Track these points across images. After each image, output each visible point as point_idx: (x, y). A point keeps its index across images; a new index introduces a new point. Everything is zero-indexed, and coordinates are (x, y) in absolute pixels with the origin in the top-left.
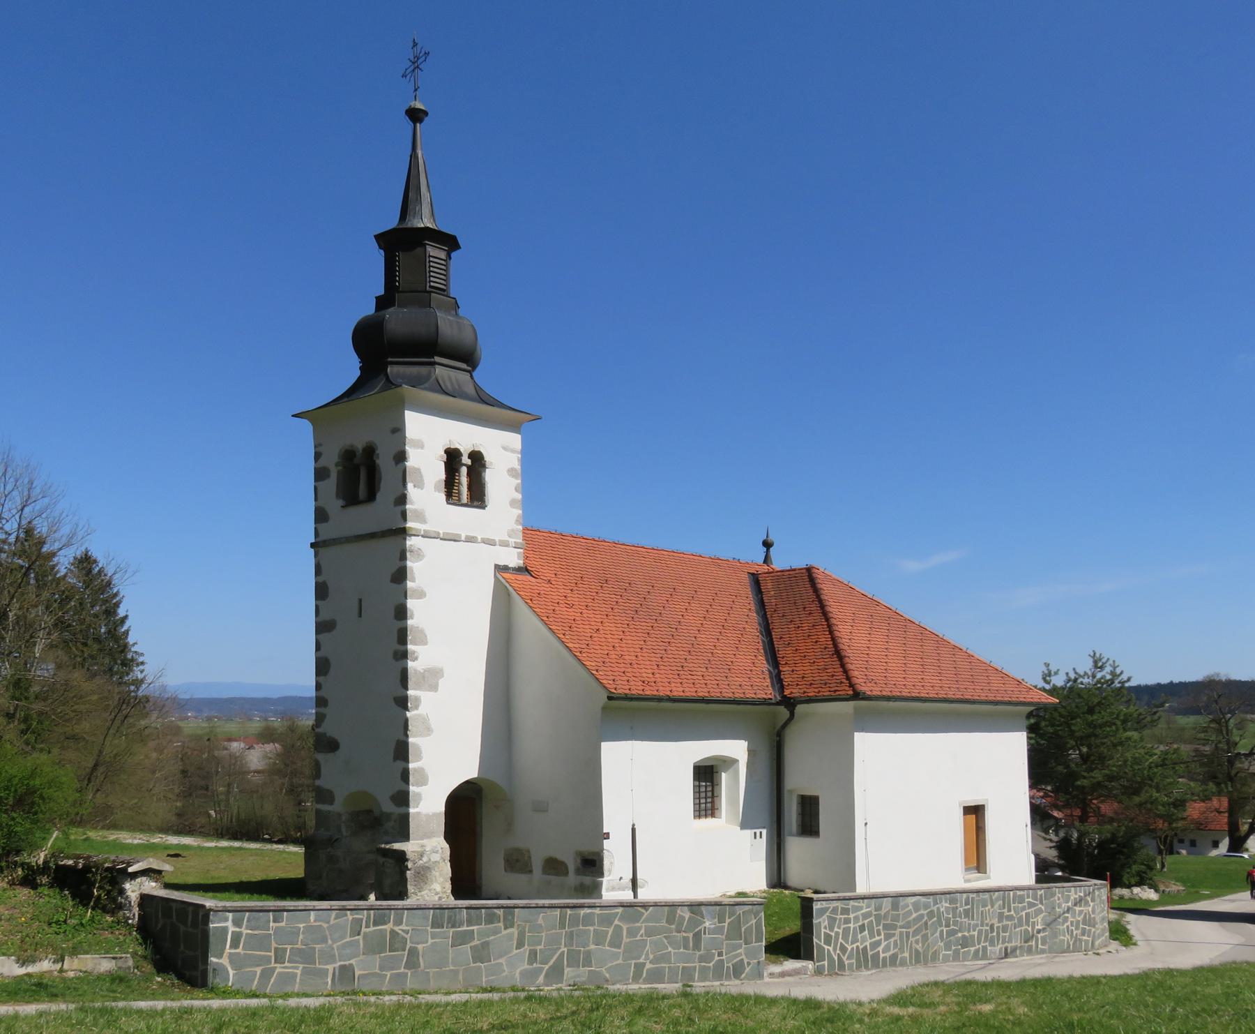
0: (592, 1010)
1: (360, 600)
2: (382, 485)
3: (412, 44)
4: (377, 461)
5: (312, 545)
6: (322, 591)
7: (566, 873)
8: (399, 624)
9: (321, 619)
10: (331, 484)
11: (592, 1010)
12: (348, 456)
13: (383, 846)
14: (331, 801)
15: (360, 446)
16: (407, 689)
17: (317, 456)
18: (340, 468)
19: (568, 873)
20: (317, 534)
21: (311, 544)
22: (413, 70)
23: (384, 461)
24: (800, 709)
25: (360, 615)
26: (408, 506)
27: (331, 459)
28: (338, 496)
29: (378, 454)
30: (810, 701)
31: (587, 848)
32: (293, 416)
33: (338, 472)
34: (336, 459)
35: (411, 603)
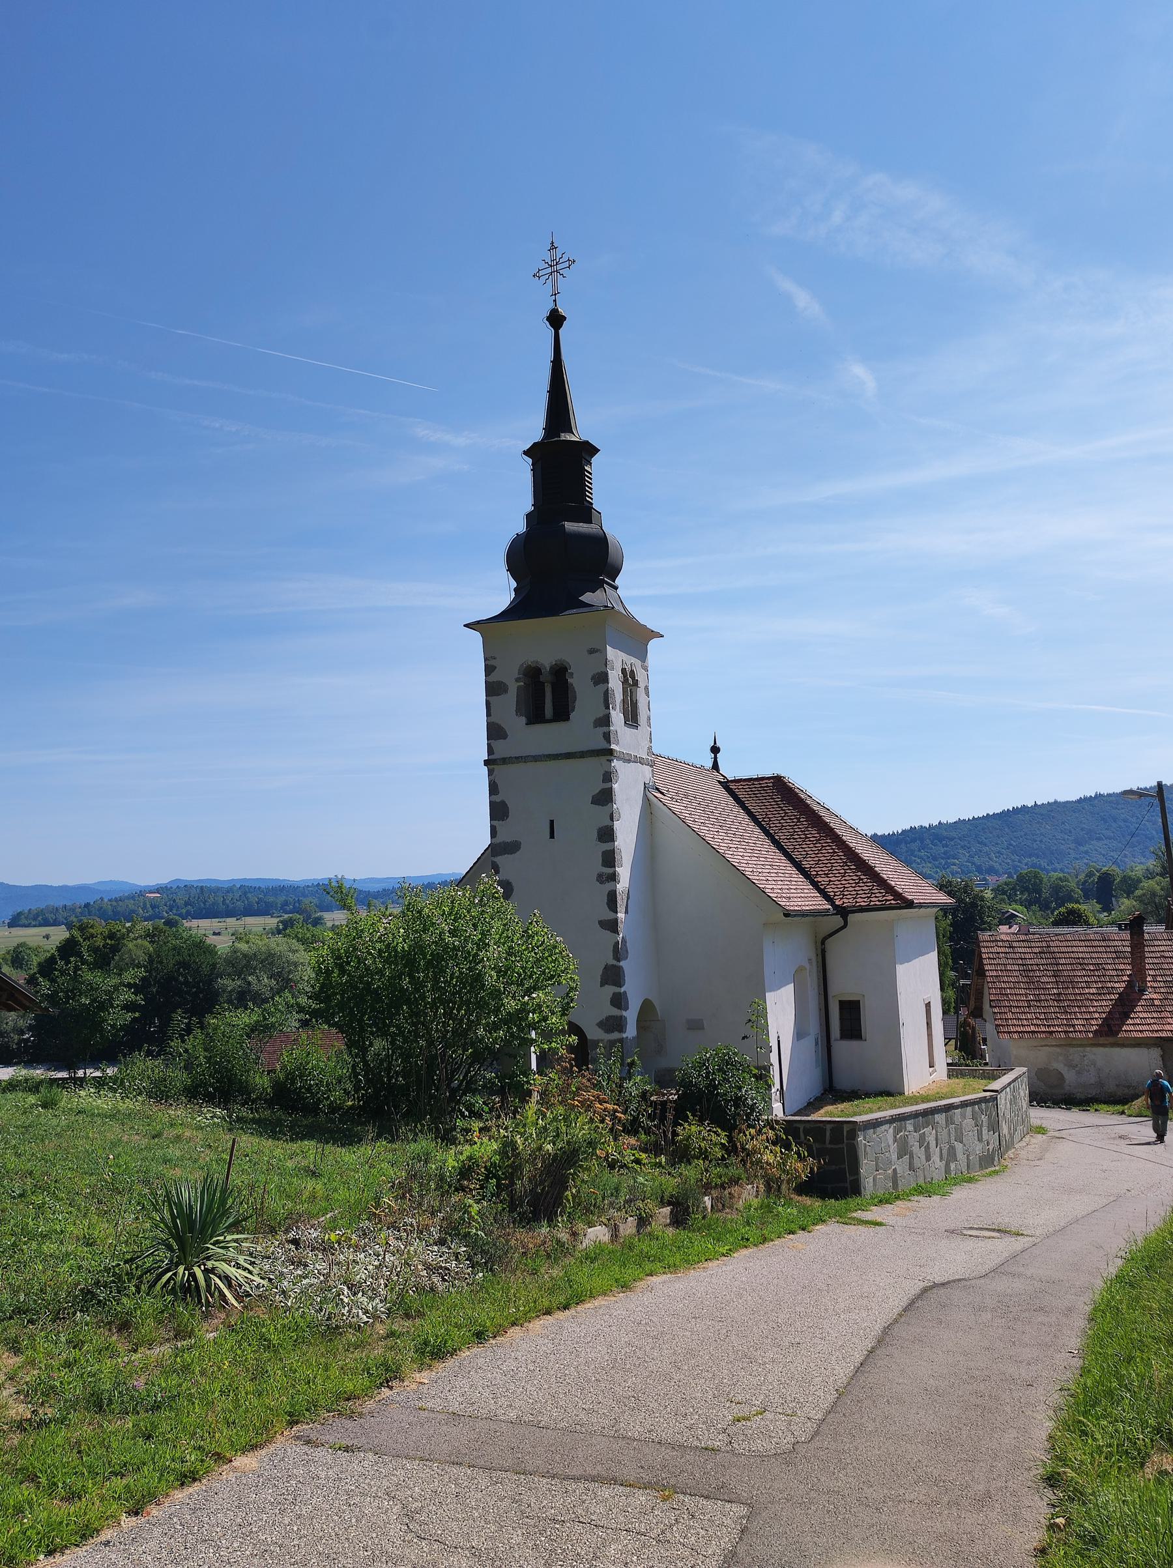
0: (307, 1056)
1: (552, 822)
2: (577, 704)
5: (486, 763)
8: (606, 847)
9: (498, 840)
11: (307, 1056)
12: (532, 674)
13: (110, 1071)
15: (546, 661)
16: (617, 913)
17: (489, 670)
20: (490, 751)
23: (579, 681)
24: (852, 918)
25: (552, 836)
26: (611, 728)
30: (862, 910)
32: (464, 626)
33: (519, 688)
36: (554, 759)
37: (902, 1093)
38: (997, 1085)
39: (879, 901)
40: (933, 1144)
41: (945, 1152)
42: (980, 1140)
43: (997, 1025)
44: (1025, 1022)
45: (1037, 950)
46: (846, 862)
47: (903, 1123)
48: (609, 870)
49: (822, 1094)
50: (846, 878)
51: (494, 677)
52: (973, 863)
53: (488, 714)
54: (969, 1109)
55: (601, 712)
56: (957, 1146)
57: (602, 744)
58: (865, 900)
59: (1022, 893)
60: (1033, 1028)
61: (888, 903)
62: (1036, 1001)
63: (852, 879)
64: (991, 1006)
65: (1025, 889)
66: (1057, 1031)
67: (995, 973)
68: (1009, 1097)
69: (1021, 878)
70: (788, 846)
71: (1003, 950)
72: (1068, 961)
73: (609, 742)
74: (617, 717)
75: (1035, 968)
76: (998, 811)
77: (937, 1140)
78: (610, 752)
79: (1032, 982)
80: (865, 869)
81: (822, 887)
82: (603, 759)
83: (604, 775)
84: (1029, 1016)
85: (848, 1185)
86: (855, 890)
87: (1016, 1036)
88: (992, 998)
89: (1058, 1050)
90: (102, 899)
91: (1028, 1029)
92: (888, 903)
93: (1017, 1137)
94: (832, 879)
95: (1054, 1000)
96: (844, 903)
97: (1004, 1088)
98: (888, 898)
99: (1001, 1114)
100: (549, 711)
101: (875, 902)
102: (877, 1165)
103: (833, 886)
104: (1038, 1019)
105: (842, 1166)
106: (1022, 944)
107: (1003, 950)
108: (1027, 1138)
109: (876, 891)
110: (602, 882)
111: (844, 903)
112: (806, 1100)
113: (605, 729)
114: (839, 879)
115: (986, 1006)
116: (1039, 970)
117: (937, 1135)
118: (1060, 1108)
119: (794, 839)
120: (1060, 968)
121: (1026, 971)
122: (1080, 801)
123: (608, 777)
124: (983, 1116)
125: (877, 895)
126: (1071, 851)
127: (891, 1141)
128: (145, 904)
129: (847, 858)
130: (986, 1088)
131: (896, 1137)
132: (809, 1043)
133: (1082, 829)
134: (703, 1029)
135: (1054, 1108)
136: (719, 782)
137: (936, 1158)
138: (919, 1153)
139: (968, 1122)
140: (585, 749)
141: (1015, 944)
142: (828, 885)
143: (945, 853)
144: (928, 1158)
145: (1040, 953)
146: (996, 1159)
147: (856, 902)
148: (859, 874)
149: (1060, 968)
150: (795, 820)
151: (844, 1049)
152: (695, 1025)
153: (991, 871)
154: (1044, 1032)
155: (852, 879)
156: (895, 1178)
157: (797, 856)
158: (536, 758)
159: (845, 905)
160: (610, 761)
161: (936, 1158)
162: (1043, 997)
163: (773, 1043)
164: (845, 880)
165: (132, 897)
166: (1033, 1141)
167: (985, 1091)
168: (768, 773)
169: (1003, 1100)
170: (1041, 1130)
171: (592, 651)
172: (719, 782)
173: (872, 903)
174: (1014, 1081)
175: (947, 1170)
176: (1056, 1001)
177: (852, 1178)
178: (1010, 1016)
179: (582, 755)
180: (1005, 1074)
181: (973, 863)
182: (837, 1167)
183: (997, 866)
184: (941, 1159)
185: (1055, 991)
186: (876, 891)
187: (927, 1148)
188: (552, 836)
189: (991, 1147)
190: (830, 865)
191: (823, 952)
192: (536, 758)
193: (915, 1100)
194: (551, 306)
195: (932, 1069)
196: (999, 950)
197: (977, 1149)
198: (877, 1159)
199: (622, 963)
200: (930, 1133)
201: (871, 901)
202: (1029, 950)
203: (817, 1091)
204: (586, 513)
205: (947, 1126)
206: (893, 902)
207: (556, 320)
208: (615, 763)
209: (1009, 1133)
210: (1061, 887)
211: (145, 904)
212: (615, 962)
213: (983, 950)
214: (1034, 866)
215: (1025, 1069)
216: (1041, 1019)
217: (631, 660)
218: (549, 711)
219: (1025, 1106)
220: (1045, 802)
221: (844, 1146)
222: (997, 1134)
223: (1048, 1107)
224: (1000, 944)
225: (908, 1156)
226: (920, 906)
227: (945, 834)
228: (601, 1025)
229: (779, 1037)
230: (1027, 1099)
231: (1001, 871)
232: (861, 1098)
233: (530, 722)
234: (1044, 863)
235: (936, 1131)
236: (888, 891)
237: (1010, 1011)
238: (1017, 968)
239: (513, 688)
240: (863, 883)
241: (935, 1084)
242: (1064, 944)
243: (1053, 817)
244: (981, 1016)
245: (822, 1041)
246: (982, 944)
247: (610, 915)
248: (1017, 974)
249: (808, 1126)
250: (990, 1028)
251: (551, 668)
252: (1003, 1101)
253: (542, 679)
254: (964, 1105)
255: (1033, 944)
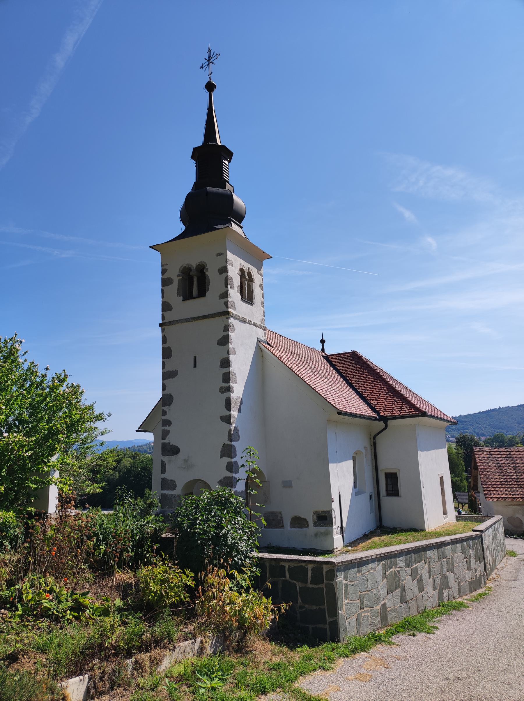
1: (195, 357)
3: (207, 51)
4: (207, 273)
5: (161, 325)
6: (166, 353)
7: (307, 526)
8: (225, 370)
9: (165, 370)
10: (174, 287)
14: (174, 488)
15: (194, 263)
16: (230, 411)
17: (164, 271)
18: (181, 278)
19: (308, 526)
20: (163, 318)
21: (160, 324)
22: (208, 64)
23: (212, 273)
24: (390, 423)
25: (195, 366)
27: (174, 274)
28: (179, 295)
29: (208, 269)
30: (396, 418)
31: (321, 508)
32: (150, 247)
33: (179, 280)
34: (177, 272)
35: (232, 357)
36: (197, 320)
37: (423, 530)
38: (482, 527)
39: (406, 412)
40: (426, 576)
41: (438, 582)
42: (469, 569)
43: (485, 494)
44: (500, 493)
45: (504, 456)
46: (388, 392)
47: (394, 560)
48: (226, 385)
49: (375, 530)
50: (387, 401)
51: (166, 276)
52: (475, 432)
53: (163, 297)
54: (459, 546)
55: (224, 289)
56: (449, 576)
57: (224, 309)
58: (398, 412)
59: (496, 443)
60: (504, 496)
61: (411, 413)
62: (505, 482)
63: (391, 401)
64: (482, 484)
65: (497, 441)
66: (517, 498)
67: (483, 467)
68: (491, 534)
69: (495, 437)
70: (356, 386)
71: (486, 456)
72: (521, 462)
73: (227, 307)
74: (234, 295)
75: (504, 465)
76: (484, 410)
77: (429, 572)
78: (228, 313)
79: (502, 472)
80: (395, 392)
81: (373, 406)
82: (224, 317)
83: (224, 327)
84: (502, 489)
85: (327, 626)
86: (392, 407)
87: (495, 500)
88: (482, 480)
89: (518, 507)
90: (134, 446)
91: (501, 496)
92: (411, 413)
93: (497, 563)
94: (379, 402)
95: (514, 481)
96: (385, 414)
97: (488, 528)
98: (411, 411)
99: (485, 547)
100: (195, 292)
101: (403, 413)
102: (362, 603)
103: (379, 405)
104: (507, 491)
105: (322, 607)
106: (496, 453)
107: (486, 456)
108: (504, 560)
109: (404, 407)
110: (222, 393)
111: (385, 414)
112: (363, 533)
113: (225, 300)
114: (383, 401)
115: (479, 485)
116: (506, 466)
117: (429, 568)
118: (521, 538)
119: (359, 382)
120: (517, 465)
121: (499, 466)
122: (519, 406)
123: (226, 328)
124: (471, 551)
125: (405, 409)
126: (516, 427)
127: (379, 578)
128: (150, 447)
129: (389, 391)
130: (475, 529)
131: (385, 574)
132: (365, 498)
133: (520, 418)
134: (292, 487)
135: (518, 538)
136: (323, 356)
137: (429, 588)
138: (411, 585)
139: (459, 556)
140: (213, 312)
141: (492, 453)
142: (376, 405)
143: (463, 427)
144: (421, 589)
145: (506, 457)
146: (483, 582)
147: (392, 413)
148: (395, 398)
149: (517, 465)
150: (361, 372)
151: (388, 502)
152: (287, 485)
153: (483, 435)
154: (510, 498)
155: (391, 401)
156: (384, 614)
157: (360, 390)
158: (187, 320)
159: (386, 415)
160: (228, 318)
161: (429, 588)
162: (509, 480)
163: (335, 495)
164: (387, 402)
165: (146, 445)
166: (509, 562)
167: (473, 531)
168: (348, 350)
169: (487, 538)
170: (513, 554)
171: (219, 255)
172: (323, 356)
173: (402, 414)
174: (494, 524)
175: (441, 596)
176: (516, 482)
177: (331, 620)
178: (492, 489)
179: (212, 316)
180: (489, 519)
181: (475, 432)
182: (318, 607)
183: (485, 433)
184: (434, 588)
185: (515, 477)
186: (404, 407)
187: (420, 580)
188: (195, 366)
189: (478, 574)
190: (392, 408)
191: (375, 444)
192: (187, 320)
193: (431, 535)
194: (208, 80)
195: (445, 516)
196: (485, 456)
197: (467, 576)
198: (362, 598)
199: (233, 443)
200: (422, 568)
201: (401, 413)
202: (499, 456)
203: (371, 527)
204: (222, 183)
205: (439, 559)
206: (414, 413)
207: (210, 87)
208: (231, 320)
209: (493, 559)
210: (513, 441)
211: (150, 447)
212: (229, 442)
213: (476, 456)
214: (501, 432)
215: (501, 517)
216: (508, 491)
217: (247, 266)
218: (195, 292)
219: (502, 539)
220: (504, 407)
221: (323, 586)
222: (482, 563)
223: (515, 538)
224: (485, 453)
225: (399, 590)
226: (432, 416)
227: (462, 420)
228: (221, 483)
229: (339, 493)
230: (503, 534)
231: (487, 435)
232: (397, 533)
233: (185, 299)
234: (505, 432)
235: (429, 566)
236: (412, 407)
237: (492, 487)
238: (494, 465)
239: (176, 280)
240: (397, 403)
241: (447, 525)
242: (518, 453)
243: (508, 413)
244: (477, 490)
245: (375, 497)
246: (475, 453)
247: (226, 413)
248: (495, 468)
249: (292, 565)
250: (482, 495)
251: (196, 267)
252: (487, 538)
253: (191, 273)
254: (454, 542)
255: (502, 453)
